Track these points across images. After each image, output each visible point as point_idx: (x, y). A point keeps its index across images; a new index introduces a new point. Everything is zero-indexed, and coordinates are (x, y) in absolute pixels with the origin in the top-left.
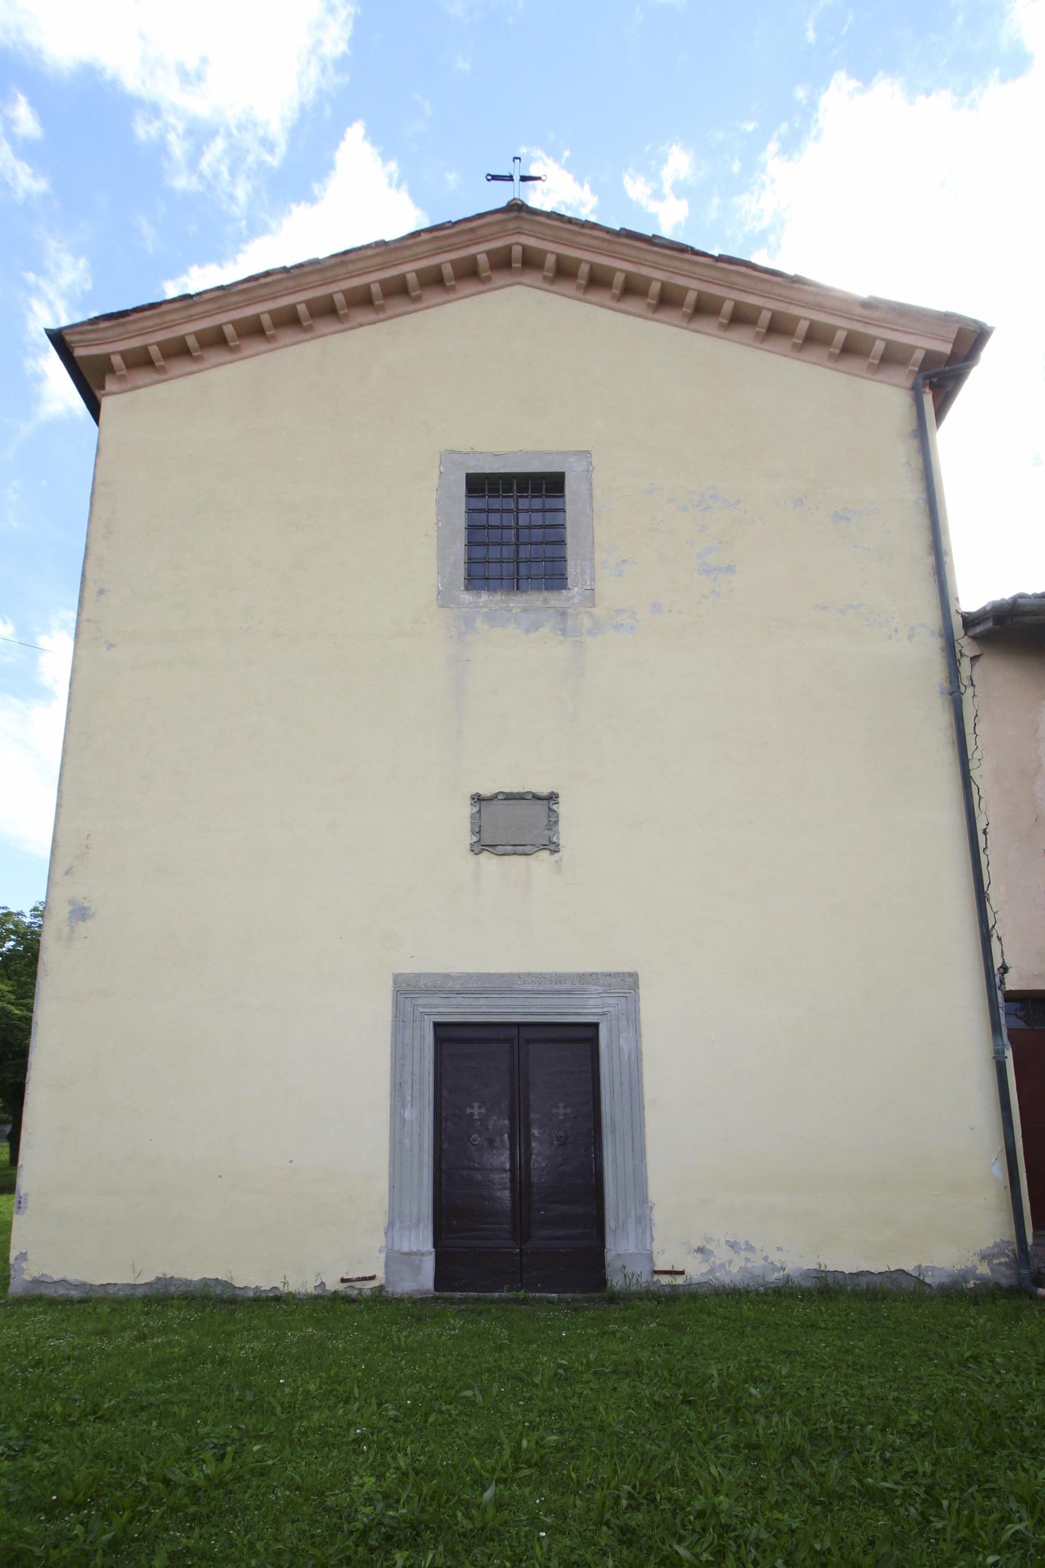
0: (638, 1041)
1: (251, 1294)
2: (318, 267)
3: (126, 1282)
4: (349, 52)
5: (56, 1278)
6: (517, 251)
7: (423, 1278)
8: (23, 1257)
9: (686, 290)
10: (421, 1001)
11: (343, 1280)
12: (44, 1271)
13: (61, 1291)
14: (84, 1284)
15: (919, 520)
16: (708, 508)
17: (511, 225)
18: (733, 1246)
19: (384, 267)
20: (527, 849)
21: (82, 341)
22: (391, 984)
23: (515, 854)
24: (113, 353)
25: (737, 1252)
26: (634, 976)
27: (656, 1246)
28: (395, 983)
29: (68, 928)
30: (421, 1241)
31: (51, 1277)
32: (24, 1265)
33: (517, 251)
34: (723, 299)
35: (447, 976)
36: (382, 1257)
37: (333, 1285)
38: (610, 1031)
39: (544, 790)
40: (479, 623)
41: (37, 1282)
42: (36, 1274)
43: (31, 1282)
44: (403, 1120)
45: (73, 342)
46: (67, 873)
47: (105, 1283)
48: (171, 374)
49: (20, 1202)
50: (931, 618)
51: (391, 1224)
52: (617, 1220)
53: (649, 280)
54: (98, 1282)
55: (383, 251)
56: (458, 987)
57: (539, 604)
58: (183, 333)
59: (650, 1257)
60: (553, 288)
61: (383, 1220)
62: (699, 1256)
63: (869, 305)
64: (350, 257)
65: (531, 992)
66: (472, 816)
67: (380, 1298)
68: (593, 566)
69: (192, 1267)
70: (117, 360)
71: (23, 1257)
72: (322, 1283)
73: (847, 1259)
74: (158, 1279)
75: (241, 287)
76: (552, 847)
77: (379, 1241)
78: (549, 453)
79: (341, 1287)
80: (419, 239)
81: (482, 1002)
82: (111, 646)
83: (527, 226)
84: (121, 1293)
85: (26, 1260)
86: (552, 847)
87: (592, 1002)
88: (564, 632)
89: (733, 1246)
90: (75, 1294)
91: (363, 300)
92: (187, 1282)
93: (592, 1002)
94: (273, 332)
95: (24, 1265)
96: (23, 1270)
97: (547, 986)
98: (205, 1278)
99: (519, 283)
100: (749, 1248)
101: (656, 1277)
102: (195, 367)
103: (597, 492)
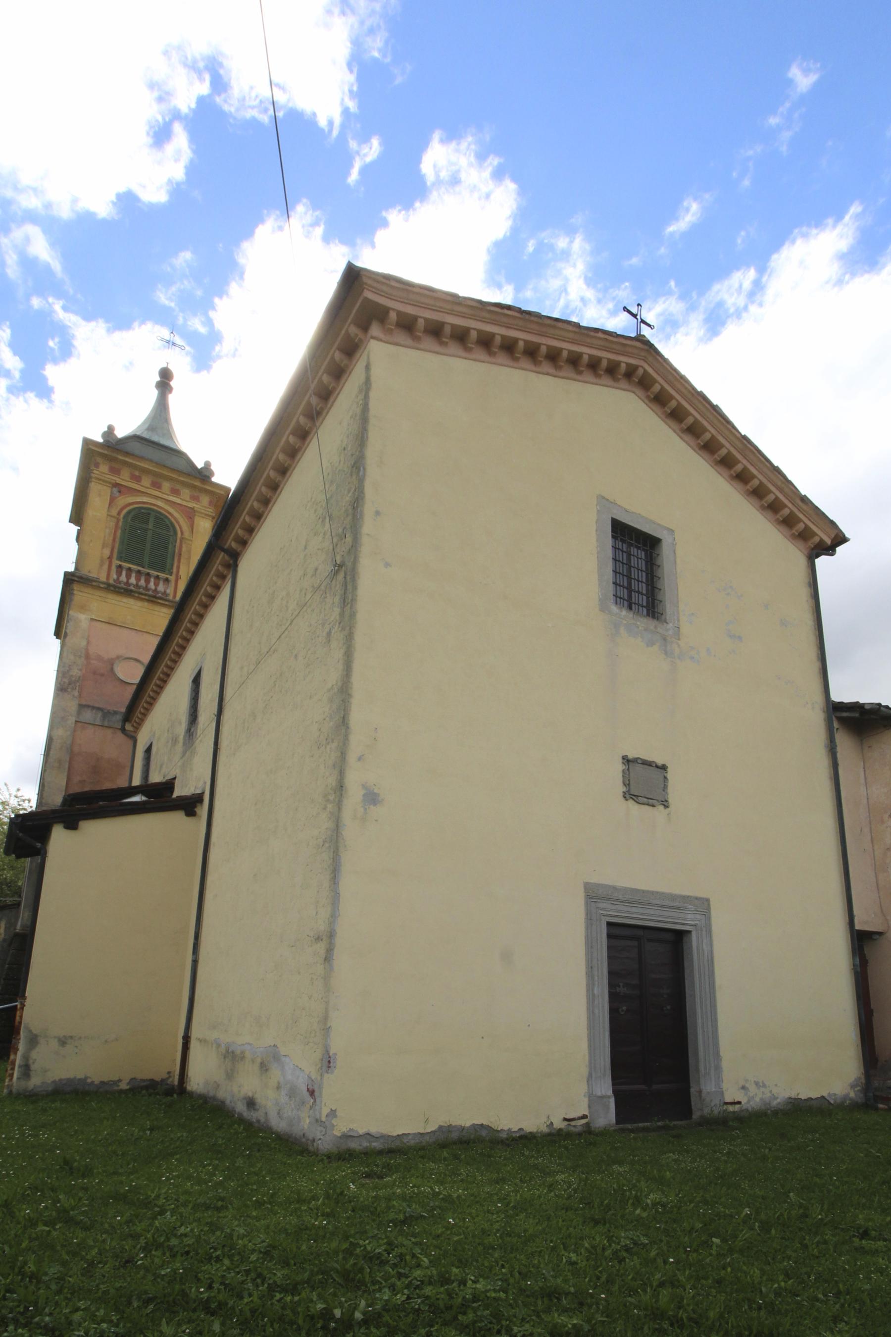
0: (711, 945)
1: (504, 1135)
2: (431, 294)
3: (416, 1131)
4: (437, 136)
5: (361, 1131)
6: (640, 372)
7: (607, 1117)
8: (333, 1113)
9: (723, 446)
10: (601, 905)
11: (565, 1119)
12: (351, 1126)
13: (365, 1144)
14: (383, 1136)
15: (812, 638)
16: (728, 594)
17: (643, 354)
18: (757, 1083)
19: (572, 342)
20: (654, 802)
21: (373, 287)
22: (583, 890)
23: (648, 805)
24: (393, 309)
25: (759, 1088)
26: (708, 900)
27: (725, 1086)
28: (585, 888)
29: (362, 810)
30: (605, 1088)
31: (357, 1131)
32: (334, 1122)
33: (640, 372)
34: (739, 462)
35: (615, 888)
36: (586, 1100)
37: (559, 1124)
38: (698, 938)
39: (660, 762)
40: (622, 630)
41: (346, 1137)
42: (344, 1130)
43: (340, 1137)
44: (594, 995)
45: (366, 284)
46: (360, 759)
47: (400, 1133)
48: (421, 346)
49: (329, 1062)
50: (819, 699)
51: (590, 1076)
52: (705, 1068)
53: (705, 430)
54: (395, 1134)
55: (454, 302)
56: (621, 897)
57: (652, 627)
58: (540, 341)
59: (722, 1093)
60: (650, 405)
61: (585, 1071)
62: (743, 1091)
63: (805, 500)
64: (560, 325)
65: (658, 905)
66: (623, 771)
67: (588, 1130)
68: (678, 613)
69: (466, 1117)
70: (393, 316)
71: (333, 1113)
72: (552, 1123)
73: (806, 1091)
74: (441, 1127)
75: (493, 308)
76: (665, 804)
77: (583, 1088)
78: (654, 523)
79: (563, 1125)
80: (596, 335)
81: (634, 910)
82: (387, 565)
83: (650, 359)
84: (413, 1142)
85: (336, 1116)
86: (665, 804)
87: (689, 916)
88: (666, 653)
89: (757, 1083)
90: (376, 1145)
91: (435, 331)
92: (463, 1129)
93: (689, 916)
94: (602, 373)
95: (334, 1122)
96: (333, 1126)
97: (667, 903)
98: (474, 1124)
99: (634, 392)
100: (764, 1086)
101: (725, 1107)
102: (438, 348)
103: (678, 561)
